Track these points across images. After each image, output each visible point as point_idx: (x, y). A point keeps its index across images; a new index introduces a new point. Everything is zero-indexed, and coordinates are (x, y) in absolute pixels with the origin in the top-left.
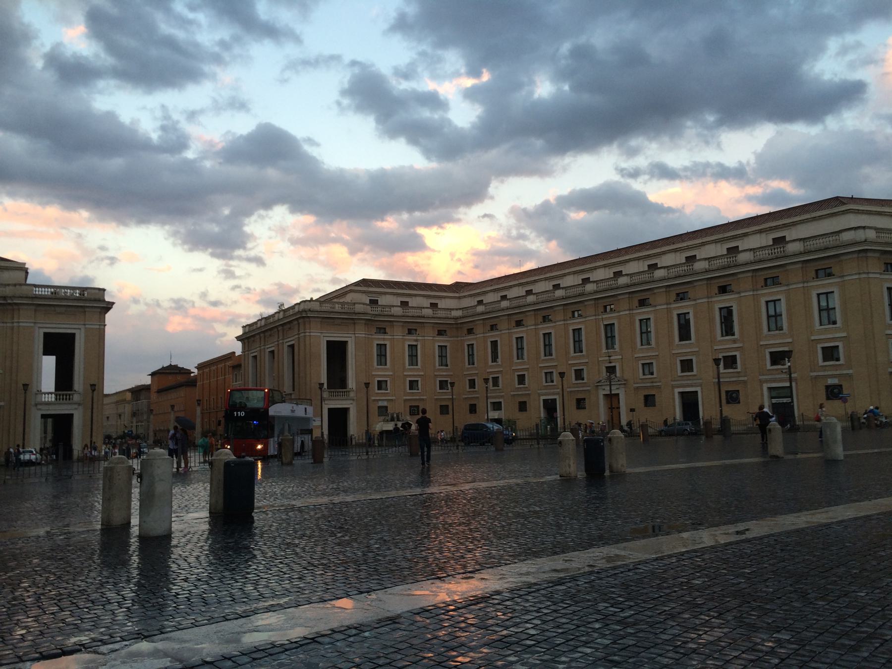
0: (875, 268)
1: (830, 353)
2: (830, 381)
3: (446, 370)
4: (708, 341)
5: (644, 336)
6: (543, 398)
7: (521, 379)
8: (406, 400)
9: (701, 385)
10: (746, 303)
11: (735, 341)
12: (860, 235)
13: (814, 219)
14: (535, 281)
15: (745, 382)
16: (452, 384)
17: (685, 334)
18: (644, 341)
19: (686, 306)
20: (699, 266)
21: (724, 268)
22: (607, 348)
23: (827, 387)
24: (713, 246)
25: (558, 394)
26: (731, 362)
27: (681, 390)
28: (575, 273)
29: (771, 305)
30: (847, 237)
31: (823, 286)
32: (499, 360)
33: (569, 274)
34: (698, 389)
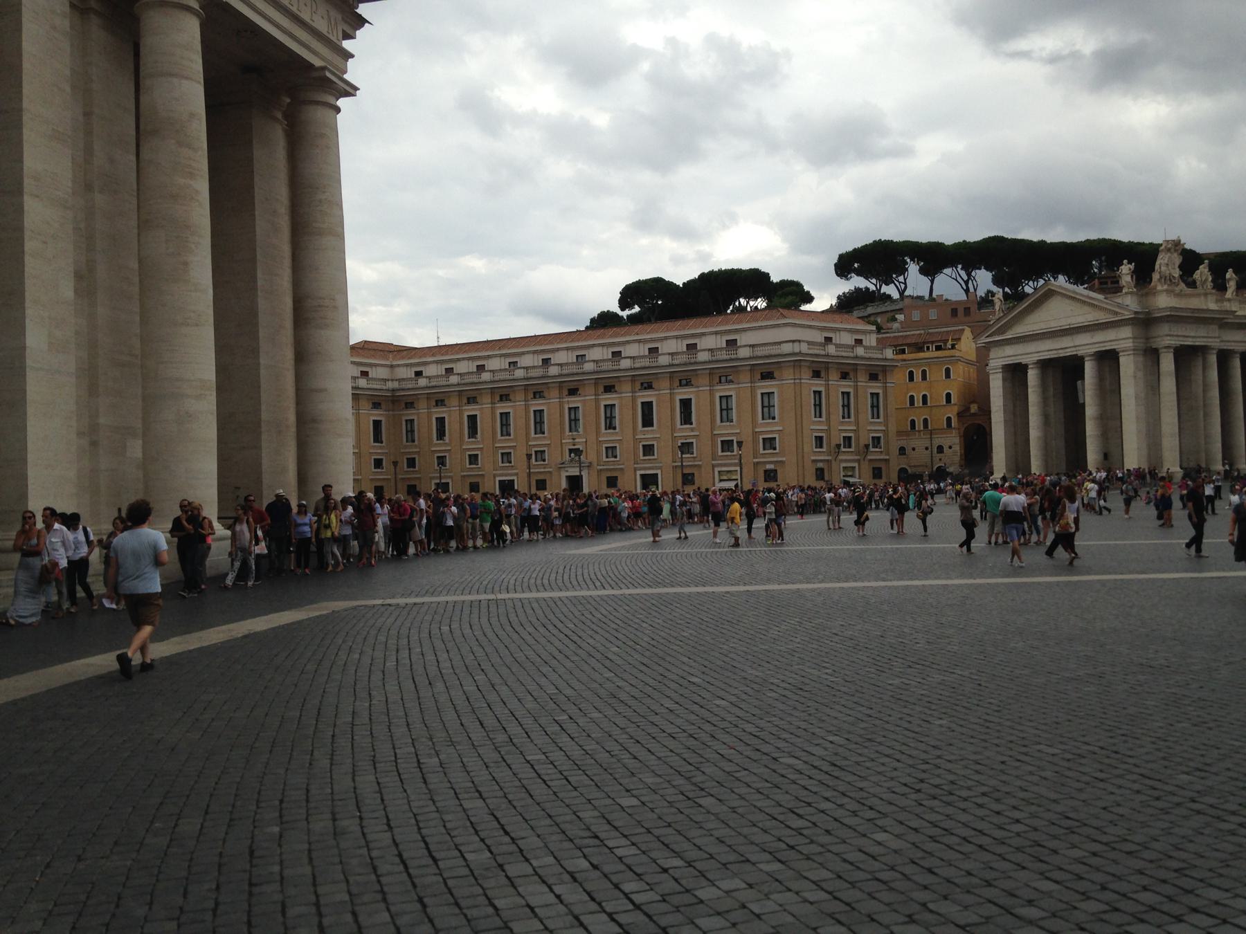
0: (806, 374)
1: (769, 443)
2: (769, 467)
3: (381, 448)
4: (628, 431)
5: (725, 413)
6: (498, 479)
7: (473, 459)
8: (814, 461)
9: (660, 468)
10: (664, 400)
11: (692, 430)
12: (796, 348)
13: (761, 328)
14: (489, 357)
15: (699, 466)
16: (740, 444)
17: (648, 422)
18: (766, 415)
19: (730, 390)
20: (554, 370)
21: (685, 364)
22: (570, 431)
23: (766, 471)
24: (531, 356)
25: (735, 465)
26: (540, 454)
27: (643, 472)
28: (534, 352)
29: (724, 401)
30: (787, 348)
31: (766, 387)
32: (447, 438)
33: (528, 352)
34: (659, 472)
